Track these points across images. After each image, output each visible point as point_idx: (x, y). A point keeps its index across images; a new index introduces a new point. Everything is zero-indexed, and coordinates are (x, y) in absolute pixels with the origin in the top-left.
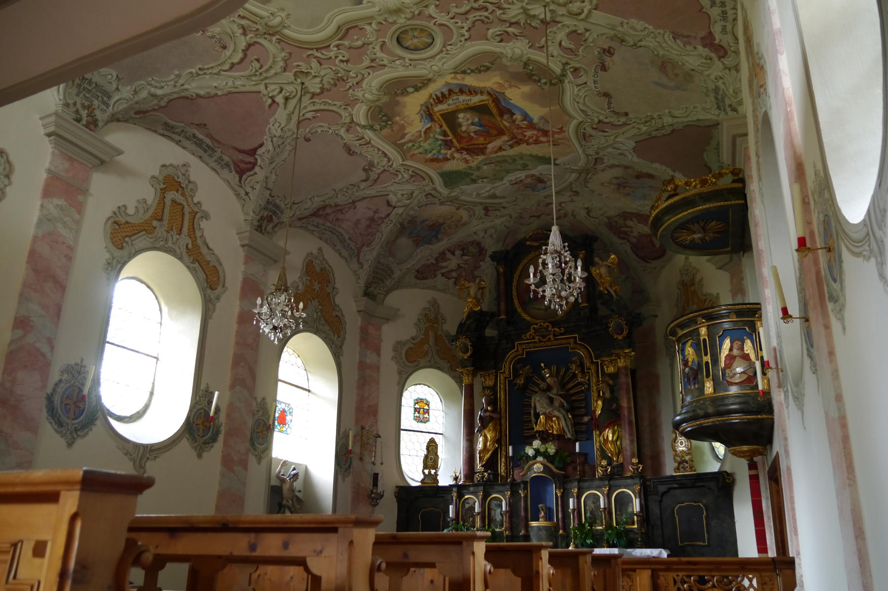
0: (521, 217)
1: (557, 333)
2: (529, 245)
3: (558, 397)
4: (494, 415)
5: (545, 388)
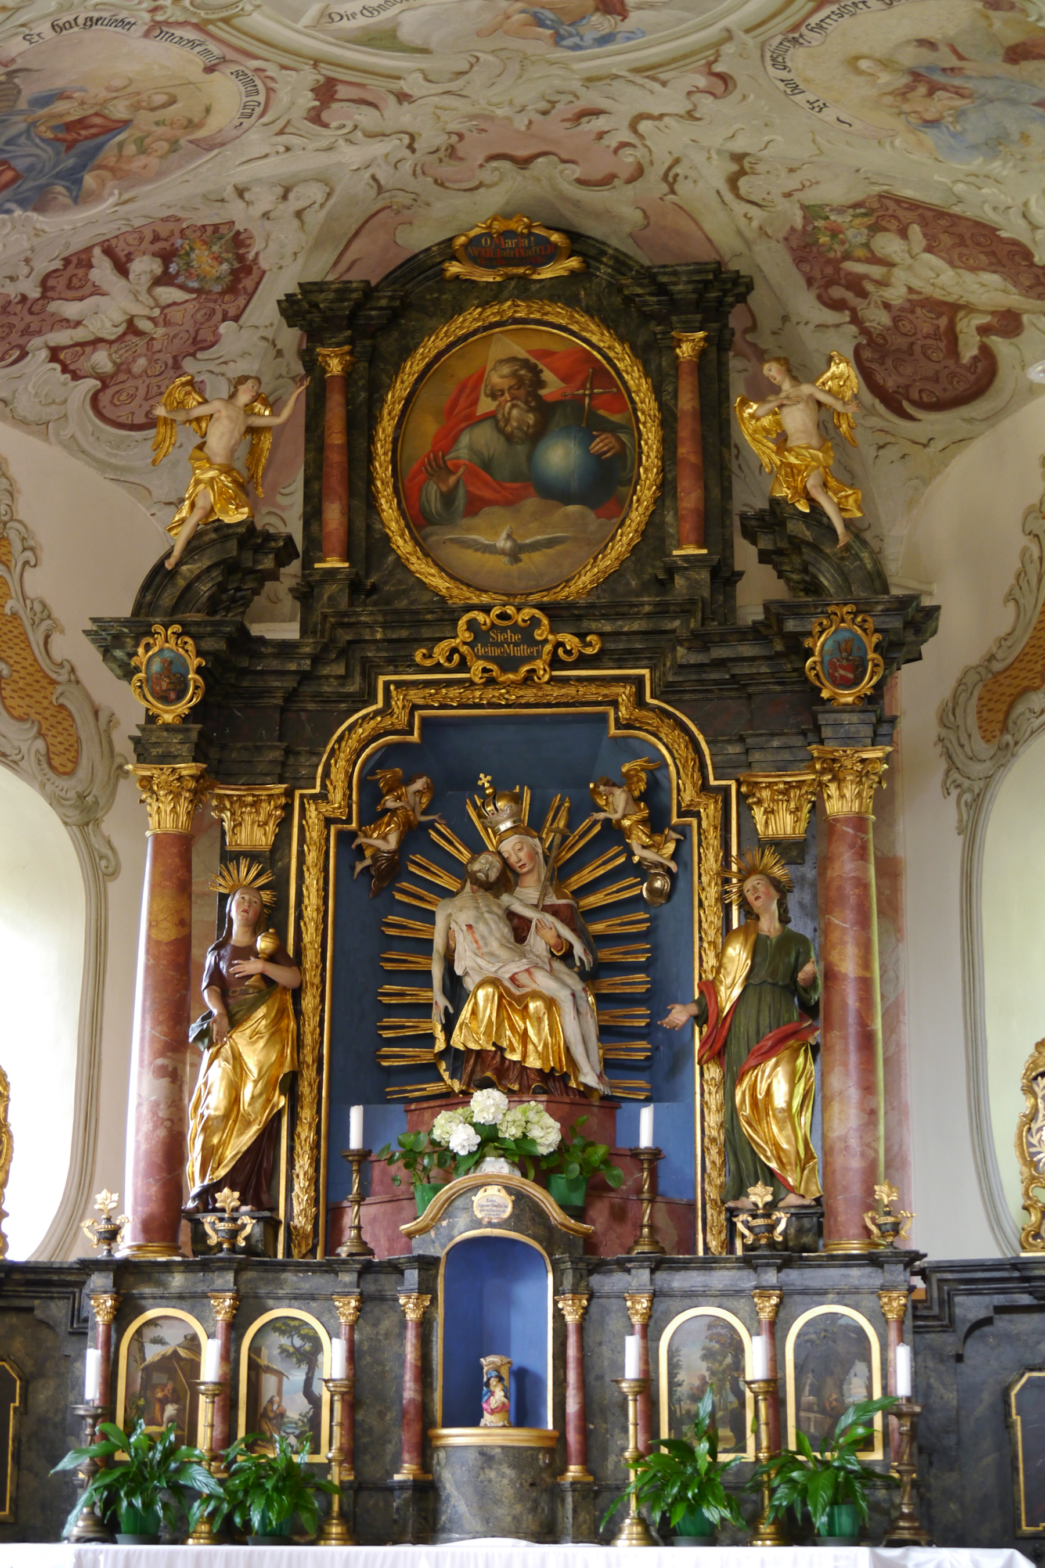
0: (452, 152)
1: (568, 653)
2: (457, 277)
3: (549, 918)
4: (277, 973)
5: (493, 875)
